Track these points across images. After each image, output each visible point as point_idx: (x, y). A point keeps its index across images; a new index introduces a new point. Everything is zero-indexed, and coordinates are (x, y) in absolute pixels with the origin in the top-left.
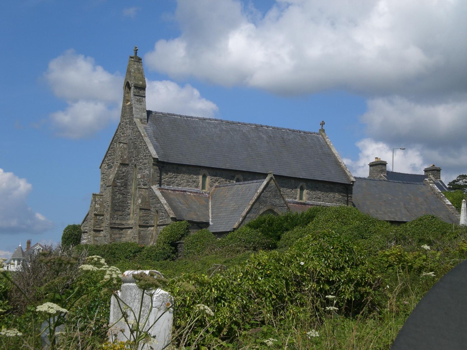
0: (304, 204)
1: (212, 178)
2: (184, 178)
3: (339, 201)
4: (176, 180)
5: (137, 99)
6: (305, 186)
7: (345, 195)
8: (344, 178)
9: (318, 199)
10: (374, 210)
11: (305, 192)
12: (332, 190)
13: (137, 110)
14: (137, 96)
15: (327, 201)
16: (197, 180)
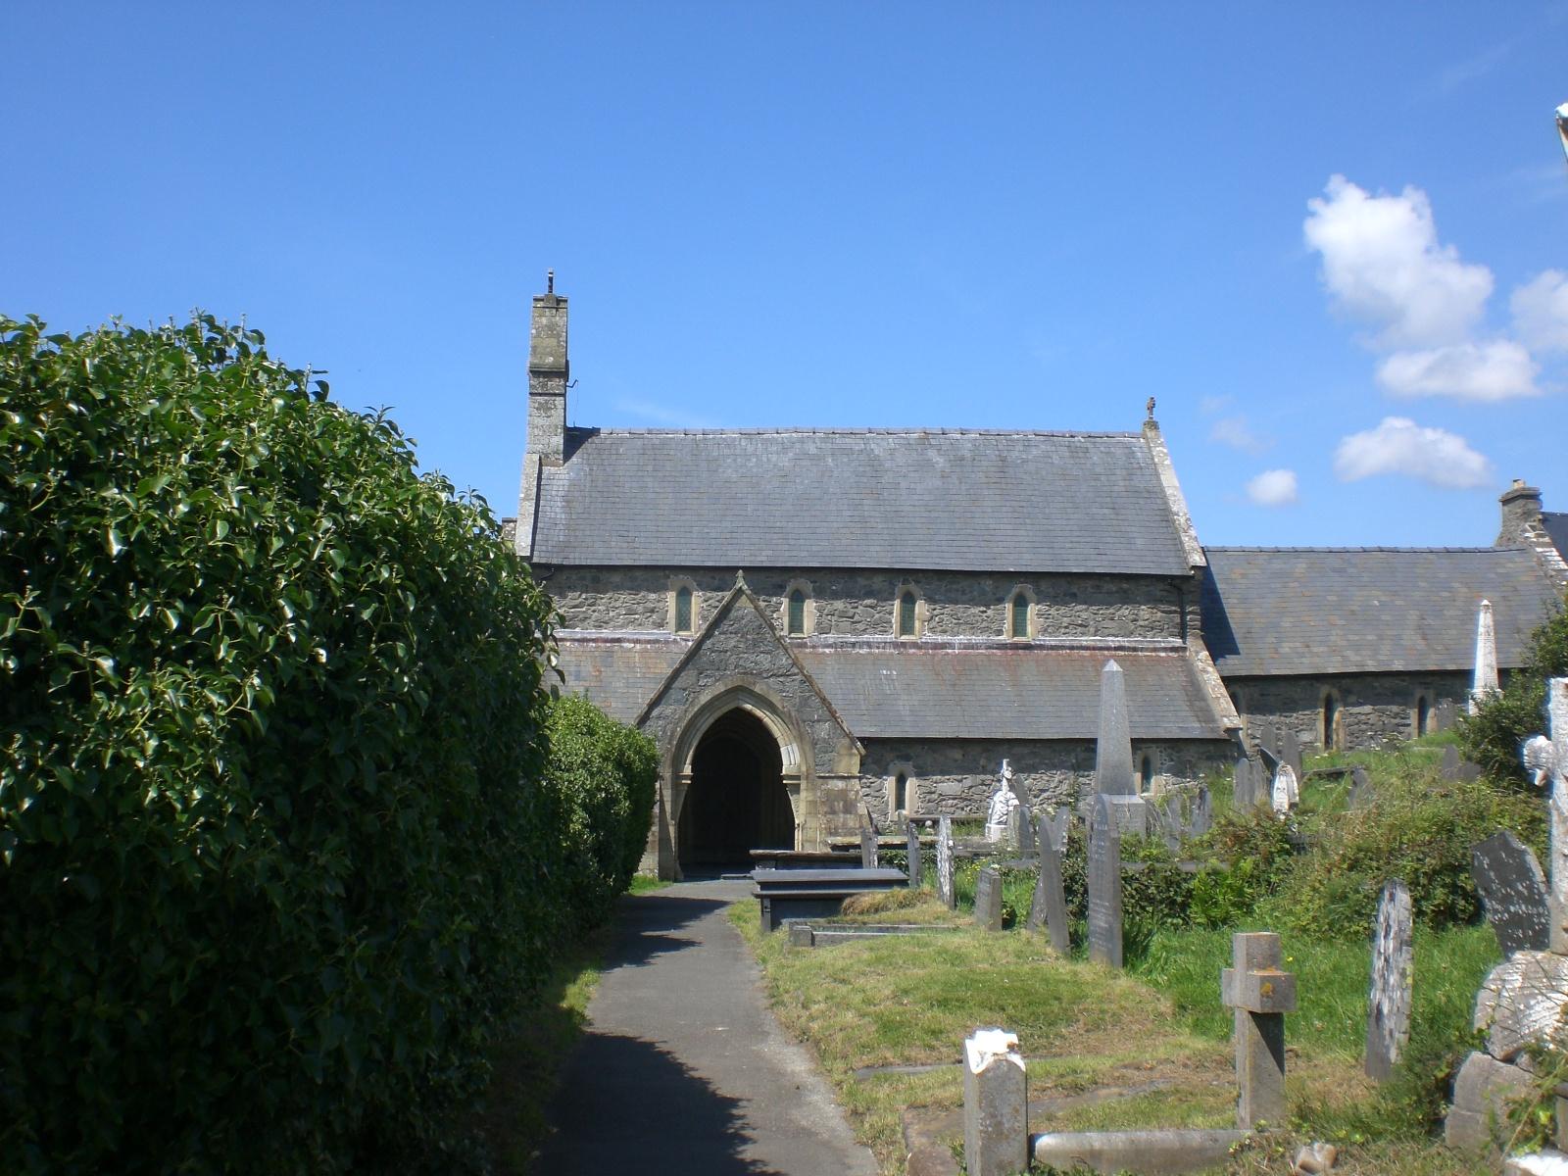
0: (1028, 647)
1: (709, 595)
2: (618, 604)
3: (1152, 629)
4: (594, 611)
5: (540, 403)
6: (1029, 592)
7: (1174, 608)
8: (1171, 560)
9: (1080, 629)
10: (1298, 644)
11: (1032, 610)
12: (1126, 599)
13: (536, 431)
14: (540, 395)
15: (1112, 631)
16: (661, 604)
